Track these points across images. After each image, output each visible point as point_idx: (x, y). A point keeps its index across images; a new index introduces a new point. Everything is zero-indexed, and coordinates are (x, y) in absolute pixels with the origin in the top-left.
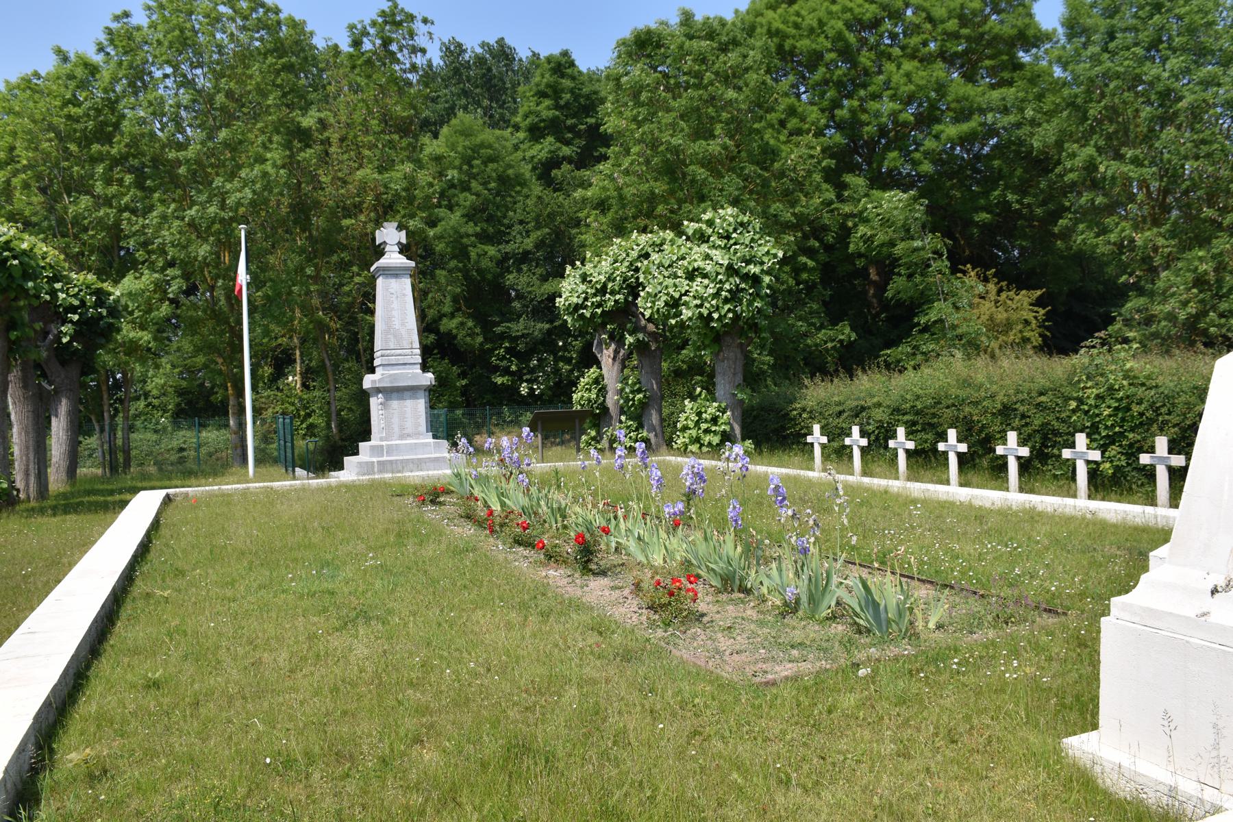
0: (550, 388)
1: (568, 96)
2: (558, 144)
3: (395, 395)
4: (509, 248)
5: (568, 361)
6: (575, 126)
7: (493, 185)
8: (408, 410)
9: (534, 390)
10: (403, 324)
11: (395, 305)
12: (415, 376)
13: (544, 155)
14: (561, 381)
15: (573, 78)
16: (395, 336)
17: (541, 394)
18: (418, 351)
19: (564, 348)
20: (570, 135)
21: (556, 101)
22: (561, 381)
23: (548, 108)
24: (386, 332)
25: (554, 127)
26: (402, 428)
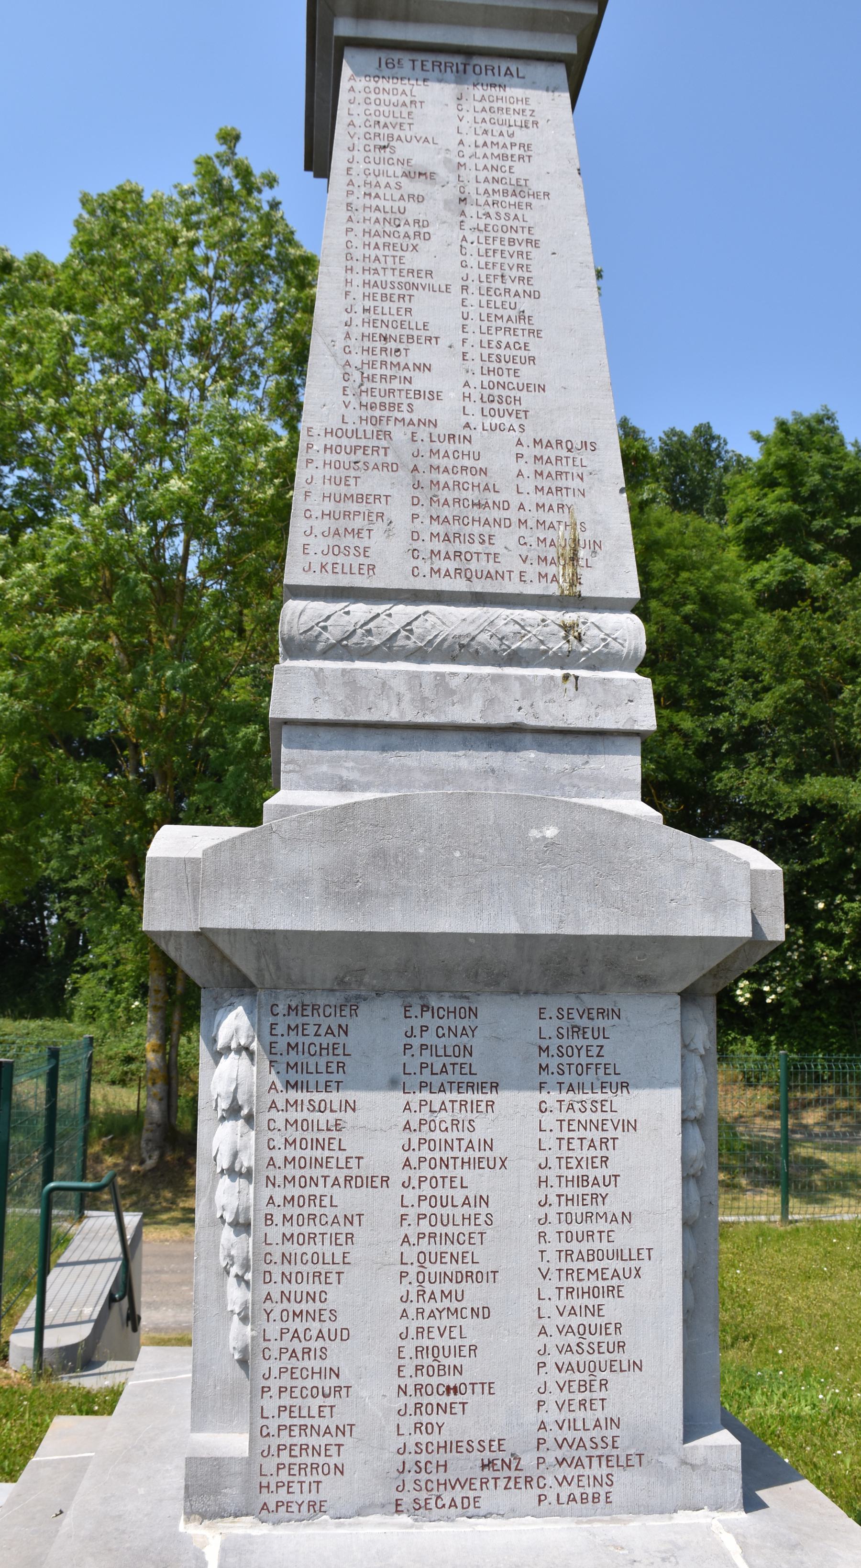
0: (796, 993)
1: (817, 477)
2: (798, 560)
3: (379, 1029)
4: (721, 721)
5: (835, 940)
6: (827, 530)
7: (689, 608)
8: (514, 1196)
9: (764, 995)
10: (501, 398)
11: (441, 252)
12: (594, 850)
13: (774, 578)
14: (817, 979)
15: (827, 450)
16: (425, 488)
17: (778, 1004)
18: (630, 632)
19: (828, 915)
20: (819, 547)
21: (793, 487)
22: (817, 979)
23: (781, 500)
24: (365, 446)
25: (791, 532)
26: (436, 1383)
